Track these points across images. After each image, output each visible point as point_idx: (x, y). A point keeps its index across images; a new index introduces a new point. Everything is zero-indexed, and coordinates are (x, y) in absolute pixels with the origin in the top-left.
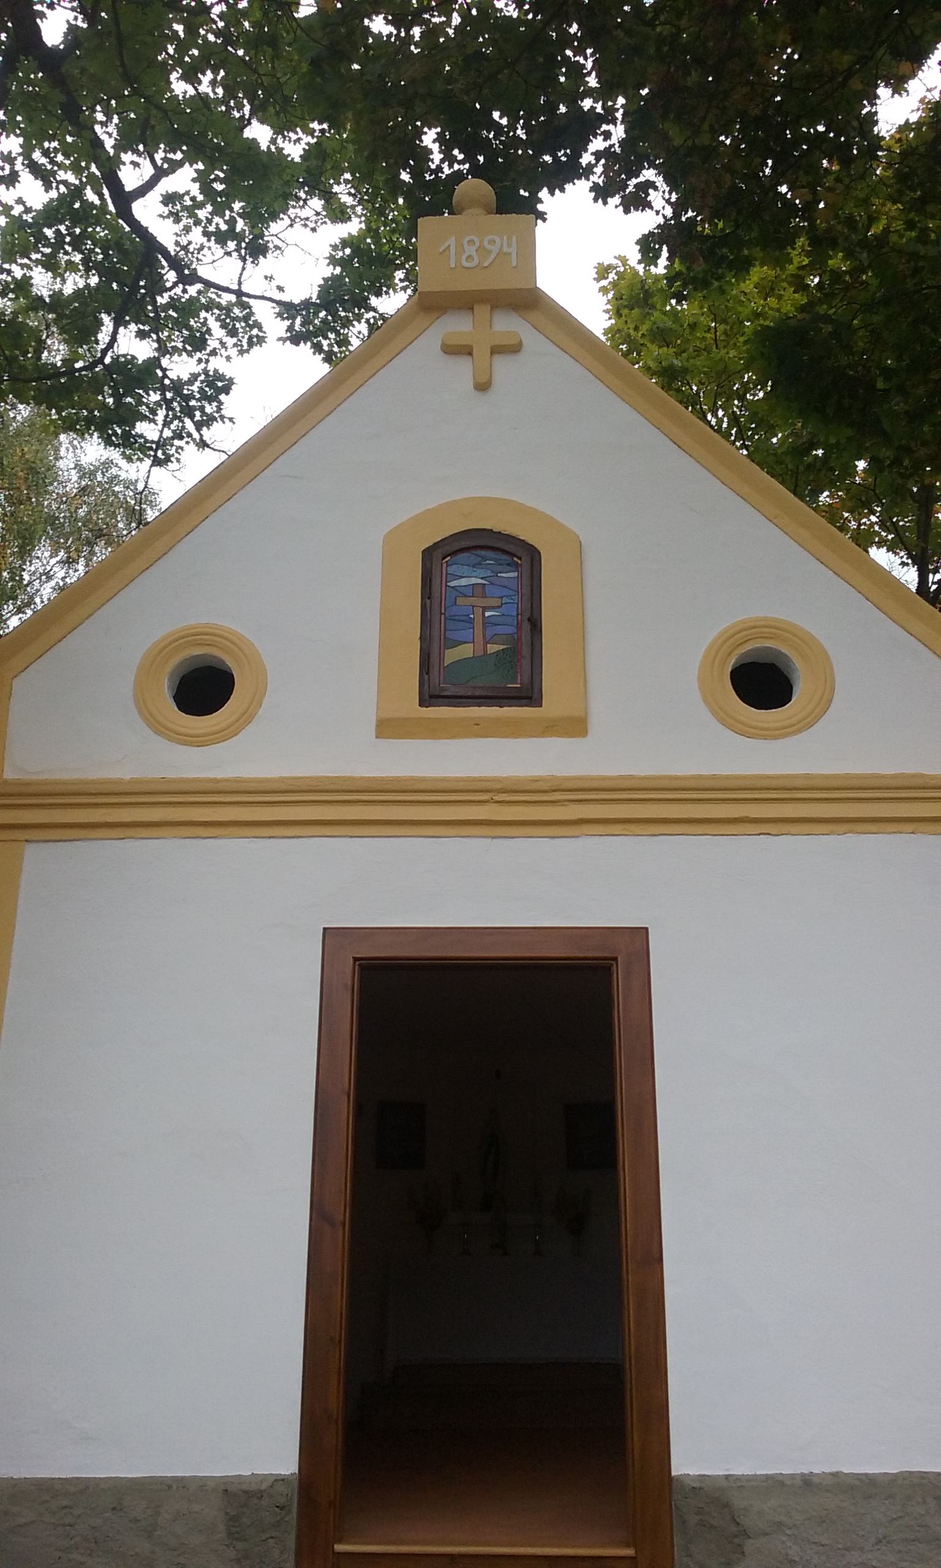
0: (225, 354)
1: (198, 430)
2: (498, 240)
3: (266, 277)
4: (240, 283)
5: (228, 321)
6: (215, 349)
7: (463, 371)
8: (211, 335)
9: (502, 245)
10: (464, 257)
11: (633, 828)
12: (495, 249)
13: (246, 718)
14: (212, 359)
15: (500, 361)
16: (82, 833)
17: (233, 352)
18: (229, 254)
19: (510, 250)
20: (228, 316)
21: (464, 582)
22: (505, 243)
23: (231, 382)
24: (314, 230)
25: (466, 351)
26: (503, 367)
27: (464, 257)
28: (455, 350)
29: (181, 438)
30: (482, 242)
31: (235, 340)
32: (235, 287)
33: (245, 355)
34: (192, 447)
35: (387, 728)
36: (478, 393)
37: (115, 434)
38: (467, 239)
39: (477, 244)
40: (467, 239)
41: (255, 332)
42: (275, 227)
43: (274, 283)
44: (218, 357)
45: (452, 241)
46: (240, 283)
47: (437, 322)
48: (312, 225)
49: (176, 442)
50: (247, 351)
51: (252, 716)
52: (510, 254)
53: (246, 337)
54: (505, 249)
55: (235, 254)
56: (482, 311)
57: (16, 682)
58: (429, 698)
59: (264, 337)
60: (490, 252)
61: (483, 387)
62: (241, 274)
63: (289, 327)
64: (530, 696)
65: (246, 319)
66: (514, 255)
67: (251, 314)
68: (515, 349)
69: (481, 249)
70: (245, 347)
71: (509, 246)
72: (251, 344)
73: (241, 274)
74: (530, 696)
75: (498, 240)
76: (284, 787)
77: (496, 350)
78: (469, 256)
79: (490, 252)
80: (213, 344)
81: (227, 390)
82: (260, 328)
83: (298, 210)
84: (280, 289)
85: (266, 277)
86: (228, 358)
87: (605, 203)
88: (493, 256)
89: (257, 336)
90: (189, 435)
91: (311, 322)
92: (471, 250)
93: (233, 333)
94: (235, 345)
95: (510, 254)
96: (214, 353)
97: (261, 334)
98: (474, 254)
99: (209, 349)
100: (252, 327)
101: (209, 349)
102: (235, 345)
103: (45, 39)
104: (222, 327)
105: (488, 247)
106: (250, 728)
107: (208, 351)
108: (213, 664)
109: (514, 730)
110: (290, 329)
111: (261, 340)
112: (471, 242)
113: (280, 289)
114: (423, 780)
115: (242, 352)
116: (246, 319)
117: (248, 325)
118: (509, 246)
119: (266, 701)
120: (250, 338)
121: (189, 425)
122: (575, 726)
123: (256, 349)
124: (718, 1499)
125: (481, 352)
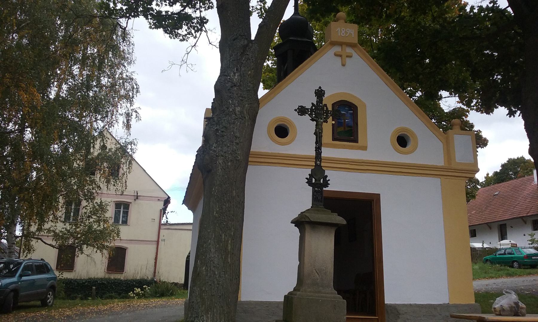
1: (195, 33)
7: (339, 59)
11: (378, 172)
15: (348, 59)
16: (259, 164)
17: (203, 9)
23: (208, 20)
26: (348, 60)
28: (336, 55)
29: (190, 34)
34: (193, 38)
37: (168, 30)
41: (211, 5)
49: (188, 36)
61: (343, 65)
64: (356, 141)
68: (351, 57)
72: (209, 8)
74: (356, 141)
77: (347, 56)
81: (206, 23)
87: (514, 116)
90: (192, 34)
92: (343, 32)
100: (210, 3)
103: (523, 122)
109: (352, 148)
115: (205, 10)
121: (193, 31)
122: (364, 148)
124: (395, 309)
125: (344, 56)
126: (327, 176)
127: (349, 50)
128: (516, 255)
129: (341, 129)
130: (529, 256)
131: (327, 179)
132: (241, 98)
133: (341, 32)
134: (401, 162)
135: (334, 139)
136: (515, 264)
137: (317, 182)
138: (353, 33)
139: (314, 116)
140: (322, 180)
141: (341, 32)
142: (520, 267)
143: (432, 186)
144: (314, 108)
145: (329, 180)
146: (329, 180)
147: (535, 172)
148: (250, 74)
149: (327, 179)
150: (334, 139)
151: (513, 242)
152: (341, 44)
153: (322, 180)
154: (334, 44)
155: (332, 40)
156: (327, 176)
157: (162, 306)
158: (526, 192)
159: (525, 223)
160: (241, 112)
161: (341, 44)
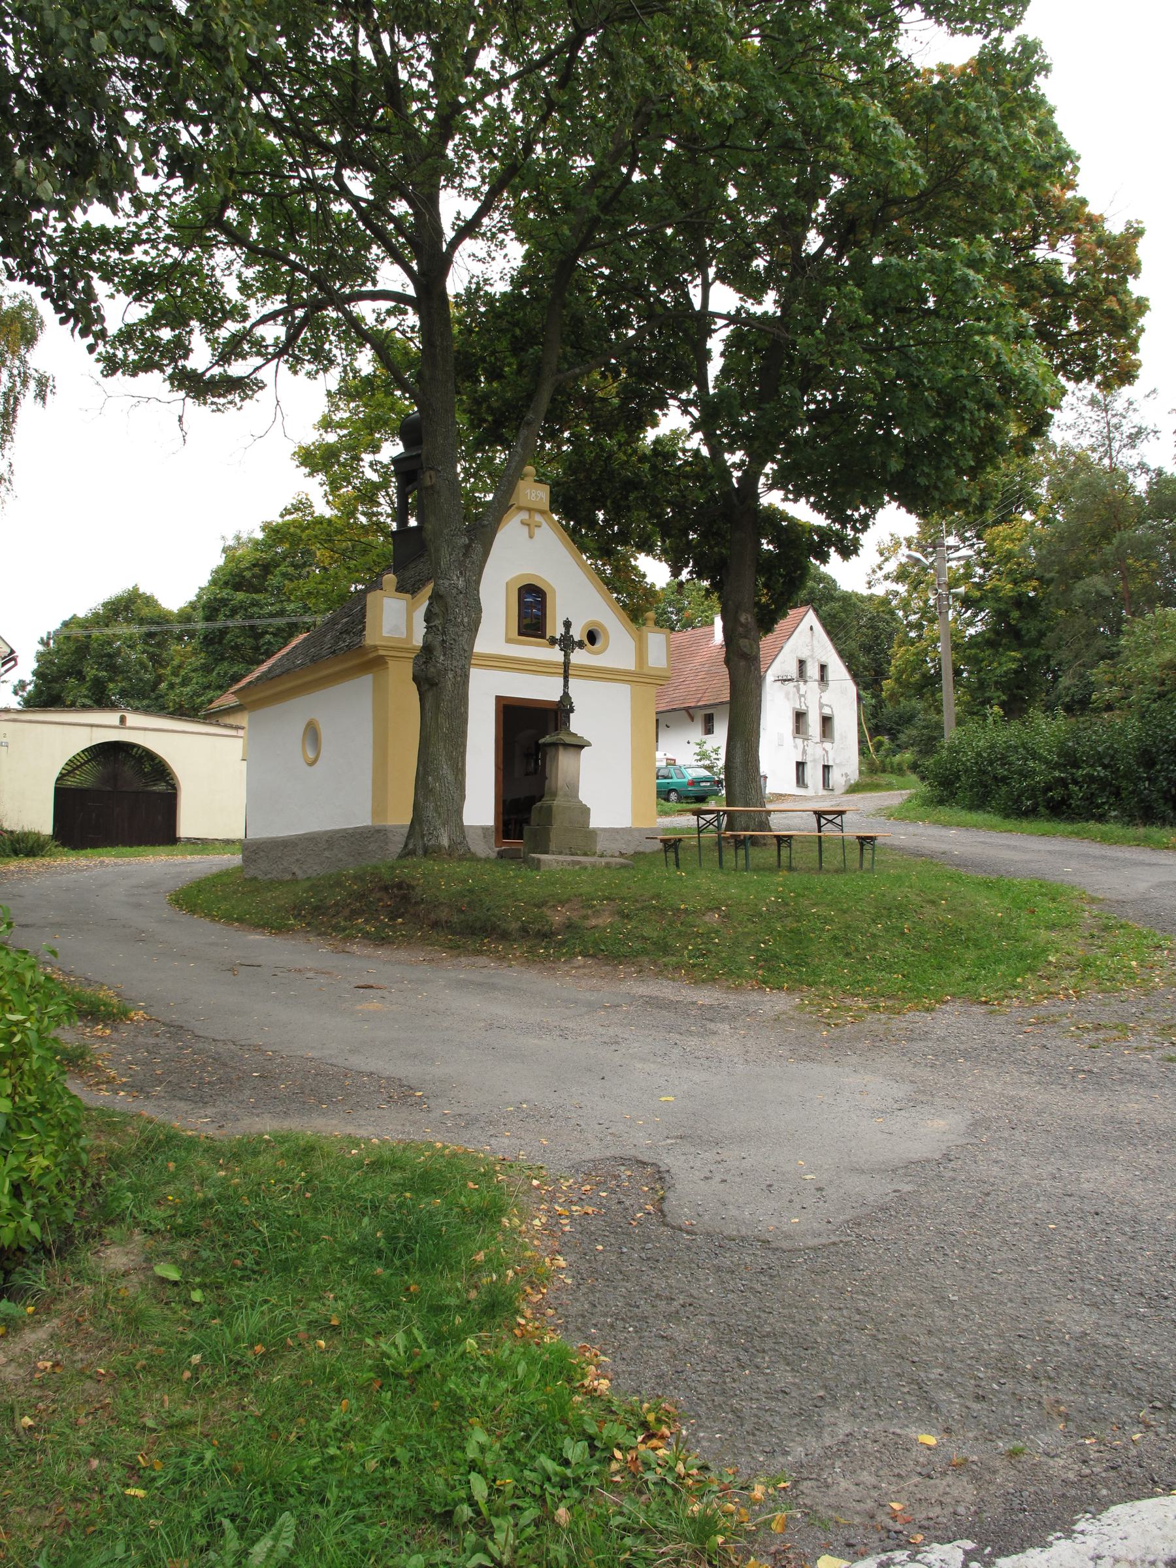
7: (526, 529)
26: (537, 530)
28: (523, 523)
61: (531, 537)
127: (538, 518)
128: (675, 780)
129: (527, 621)
130: (694, 782)
135: (520, 634)
136: (673, 796)
142: (679, 800)
143: (621, 693)
147: (718, 622)
150: (520, 634)
151: (669, 756)
152: (530, 510)
154: (520, 509)
157: (129, 864)
158: (698, 660)
159: (692, 719)
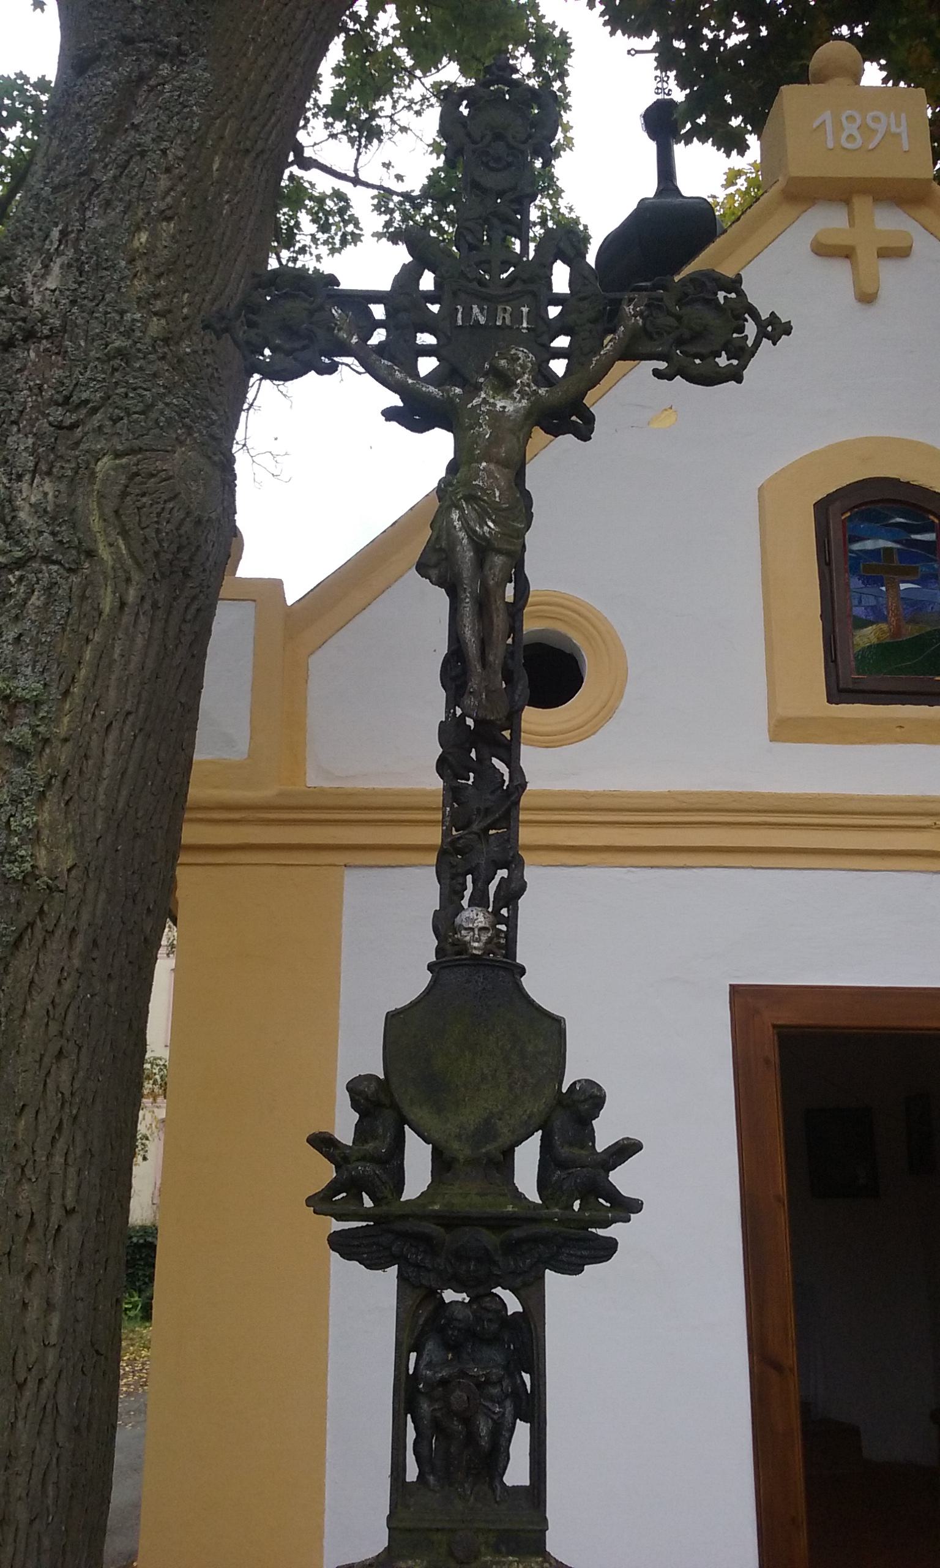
0: (315, 252)
2: (883, 118)
3: (384, 165)
4: (356, 170)
5: (321, 215)
6: (305, 246)
7: (840, 273)
8: (300, 229)
9: (889, 125)
10: (844, 136)
12: (881, 128)
13: (606, 712)
14: (300, 257)
17: (324, 250)
18: (333, 136)
19: (898, 131)
20: (321, 208)
21: (869, 545)
22: (893, 120)
24: (418, 113)
25: (847, 253)
26: (889, 273)
27: (844, 136)
28: (823, 250)
30: (864, 118)
31: (326, 236)
32: (353, 175)
33: (336, 255)
35: (785, 729)
36: (857, 305)
38: (849, 112)
39: (859, 122)
40: (849, 112)
41: (350, 228)
42: (384, 104)
43: (393, 172)
44: (308, 255)
45: (827, 115)
46: (356, 170)
47: (805, 217)
48: (416, 107)
50: (339, 251)
51: (613, 710)
52: (899, 134)
53: (340, 234)
54: (893, 129)
55: (344, 138)
56: (861, 204)
57: (313, 660)
58: (838, 693)
59: (360, 235)
60: (874, 131)
61: (867, 298)
62: (357, 160)
63: (386, 222)
65: (342, 212)
66: (904, 136)
67: (348, 207)
68: (902, 253)
69: (863, 128)
70: (338, 246)
71: (898, 125)
72: (344, 242)
73: (357, 160)
75: (883, 118)
76: (673, 804)
77: (885, 253)
78: (850, 136)
79: (874, 131)
80: (303, 239)
82: (357, 225)
83: (402, 90)
84: (399, 178)
85: (384, 165)
86: (319, 258)
88: (879, 136)
89: (352, 233)
91: (412, 218)
92: (851, 128)
93: (324, 228)
94: (326, 242)
95: (899, 134)
96: (303, 250)
97: (357, 231)
98: (856, 134)
99: (298, 246)
100: (346, 223)
101: (298, 246)
102: (326, 242)
104: (313, 221)
105: (872, 125)
106: (610, 728)
107: (296, 248)
108: (544, 642)
110: (388, 224)
111: (356, 238)
112: (851, 118)
113: (399, 178)
114: (851, 798)
115: (333, 251)
116: (342, 212)
117: (343, 220)
118: (898, 125)
119: (628, 689)
120: (344, 235)
123: (350, 248)
125: (866, 254)
126: (590, 1099)
127: (890, 222)
131: (603, 1141)
132: (57, 414)
133: (838, 127)
134: (785, 790)
137: (469, 1197)
138: (903, 129)
139: (427, 365)
140: (527, 1159)
141: (838, 127)
144: (427, 282)
145: (626, 1150)
146: (626, 1150)
148: (150, 251)
149: (603, 1141)
150: (838, 693)
153: (527, 1159)
155: (793, 175)
156: (590, 1099)
160: (57, 516)
161: (842, 192)
